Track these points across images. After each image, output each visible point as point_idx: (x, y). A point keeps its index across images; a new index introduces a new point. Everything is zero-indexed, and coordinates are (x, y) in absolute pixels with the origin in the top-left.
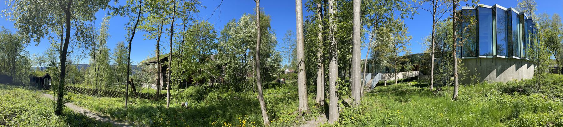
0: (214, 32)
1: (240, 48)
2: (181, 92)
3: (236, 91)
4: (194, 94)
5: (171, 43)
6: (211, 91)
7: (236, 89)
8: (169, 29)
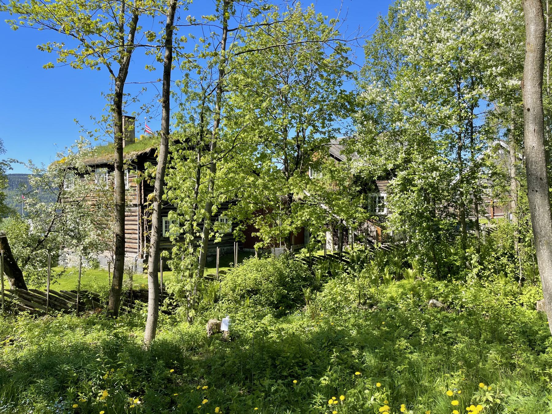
0: (339, 50)
1: (445, 102)
2: (211, 278)
3: (439, 277)
4: (265, 286)
5: (167, 93)
6: (332, 275)
7: (437, 268)
8: (162, 33)
